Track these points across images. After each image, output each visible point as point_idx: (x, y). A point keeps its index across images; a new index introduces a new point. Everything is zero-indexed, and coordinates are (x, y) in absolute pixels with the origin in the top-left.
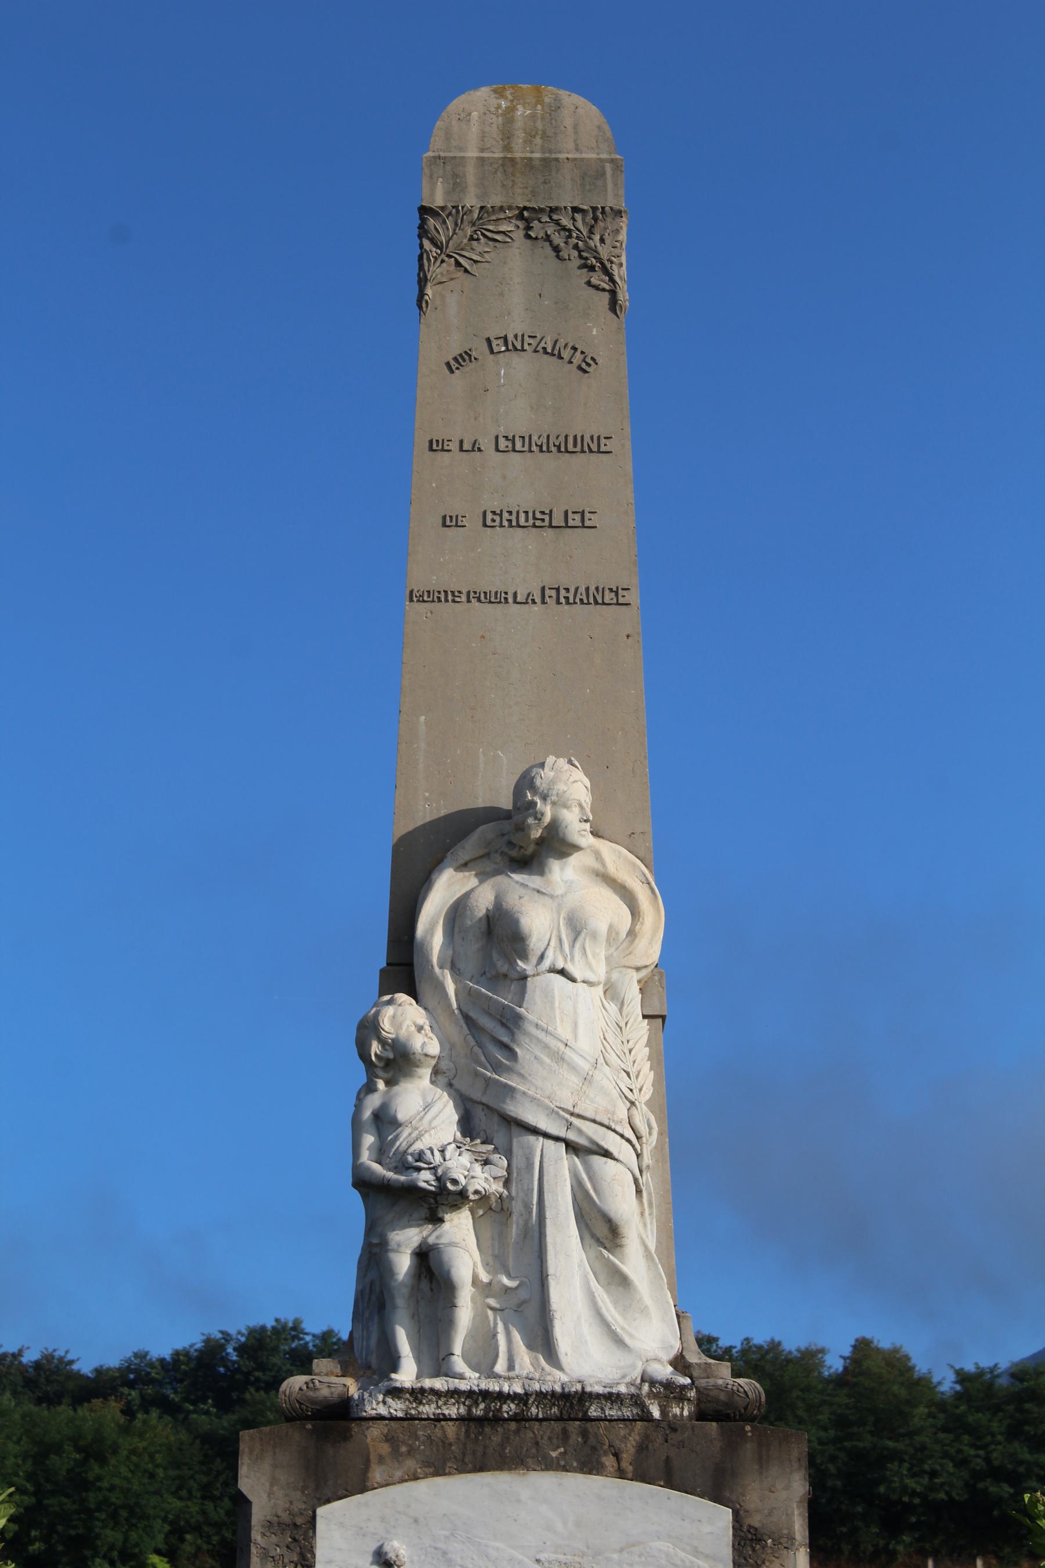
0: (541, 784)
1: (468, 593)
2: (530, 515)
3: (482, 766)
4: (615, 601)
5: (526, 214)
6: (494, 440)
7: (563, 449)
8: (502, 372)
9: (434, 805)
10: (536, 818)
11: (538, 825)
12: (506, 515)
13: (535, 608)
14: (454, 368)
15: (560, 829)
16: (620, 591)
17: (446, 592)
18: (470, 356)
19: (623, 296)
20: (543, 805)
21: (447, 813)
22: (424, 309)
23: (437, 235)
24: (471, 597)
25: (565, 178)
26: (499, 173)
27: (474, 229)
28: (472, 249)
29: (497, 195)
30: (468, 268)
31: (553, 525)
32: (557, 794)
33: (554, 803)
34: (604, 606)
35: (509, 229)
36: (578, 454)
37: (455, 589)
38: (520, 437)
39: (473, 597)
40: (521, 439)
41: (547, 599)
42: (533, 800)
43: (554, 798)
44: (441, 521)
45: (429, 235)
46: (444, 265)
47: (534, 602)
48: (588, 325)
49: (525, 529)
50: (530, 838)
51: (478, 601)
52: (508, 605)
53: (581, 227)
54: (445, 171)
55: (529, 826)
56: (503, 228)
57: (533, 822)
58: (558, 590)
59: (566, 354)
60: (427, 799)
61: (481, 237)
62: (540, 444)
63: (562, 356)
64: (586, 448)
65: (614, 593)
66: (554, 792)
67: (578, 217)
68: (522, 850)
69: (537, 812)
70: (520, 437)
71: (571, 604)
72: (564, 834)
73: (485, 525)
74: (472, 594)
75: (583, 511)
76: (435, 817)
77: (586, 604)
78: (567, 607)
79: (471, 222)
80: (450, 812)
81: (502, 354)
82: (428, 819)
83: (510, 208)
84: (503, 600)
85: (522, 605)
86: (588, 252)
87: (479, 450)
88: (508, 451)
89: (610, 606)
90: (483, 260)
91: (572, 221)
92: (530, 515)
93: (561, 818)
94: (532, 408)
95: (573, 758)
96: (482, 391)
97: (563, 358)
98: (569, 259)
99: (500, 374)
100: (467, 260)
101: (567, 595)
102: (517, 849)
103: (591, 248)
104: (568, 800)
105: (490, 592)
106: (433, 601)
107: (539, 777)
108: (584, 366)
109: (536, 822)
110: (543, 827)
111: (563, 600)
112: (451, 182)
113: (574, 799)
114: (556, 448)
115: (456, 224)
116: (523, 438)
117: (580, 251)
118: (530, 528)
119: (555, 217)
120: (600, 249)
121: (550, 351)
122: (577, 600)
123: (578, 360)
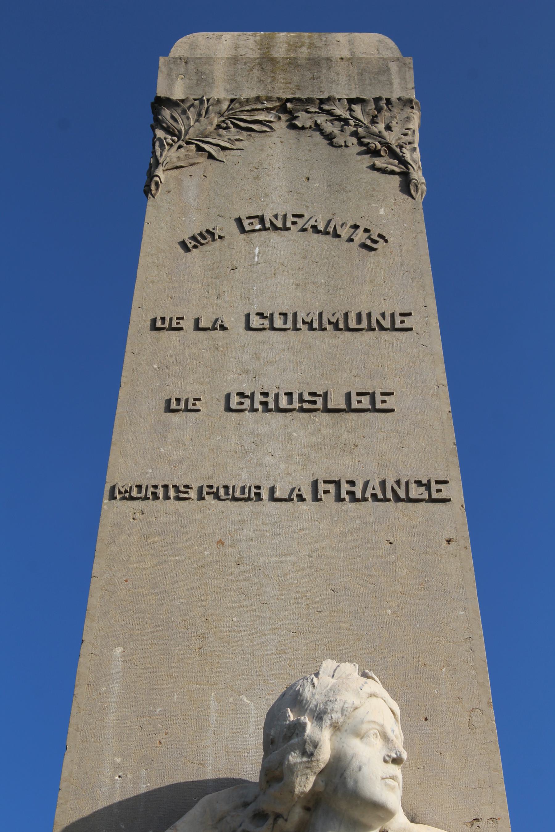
0: (313, 695)
1: (200, 489)
2: (296, 397)
3: (213, 717)
4: (426, 496)
5: (289, 105)
6: (244, 318)
7: (341, 325)
8: (257, 251)
9: (130, 776)
10: (304, 753)
11: (309, 766)
12: (259, 398)
13: (303, 506)
14: (190, 246)
15: (348, 772)
16: (433, 484)
17: (166, 487)
18: (212, 234)
19: (418, 175)
20: (317, 729)
21: (151, 789)
22: (153, 192)
23: (175, 124)
24: (204, 492)
25: (338, 74)
26: (255, 71)
27: (222, 119)
28: (220, 136)
29: (252, 89)
30: (214, 153)
31: (329, 407)
32: (342, 710)
33: (336, 727)
34: (410, 504)
35: (267, 119)
36: (364, 332)
37: (180, 484)
38: (280, 314)
39: (208, 493)
40: (282, 317)
41: (321, 493)
42: (298, 720)
43: (336, 716)
44: (163, 406)
45: (164, 125)
46: (182, 150)
47: (301, 498)
48: (374, 205)
49: (287, 415)
50: (292, 792)
51: (214, 498)
52: (261, 502)
53: (360, 116)
54: (187, 70)
55: (291, 769)
56: (261, 117)
57: (299, 760)
58: (338, 484)
59: (345, 233)
60: (117, 767)
61: (231, 126)
62: (309, 321)
63: (338, 233)
64: (374, 324)
65: (424, 488)
66: (337, 706)
67: (357, 108)
68: (280, 821)
69: (305, 742)
70: (280, 314)
71: (358, 500)
72: (356, 782)
73: (228, 409)
74: (206, 490)
75: (374, 393)
76: (130, 794)
77: (381, 500)
78: (353, 505)
79: (219, 113)
80: (155, 787)
81: (256, 234)
82: (118, 798)
83: (269, 99)
84: (252, 495)
85: (283, 503)
86: (369, 137)
87: (223, 328)
88: (264, 329)
89: (418, 504)
90: (233, 147)
91: (348, 113)
92: (296, 397)
93: (350, 752)
94: (298, 286)
95: (367, 671)
96: (228, 270)
97: (339, 236)
98: (346, 146)
99: (254, 252)
100: (213, 147)
101: (352, 489)
102: (270, 821)
103: (374, 134)
104: (362, 722)
105: (234, 487)
106: (146, 498)
107: (309, 684)
108: (369, 242)
109: (305, 759)
110: (318, 770)
111: (344, 495)
112: (194, 78)
113: (374, 722)
114: (332, 326)
115: (199, 115)
116: (285, 315)
117: (359, 138)
118: (295, 412)
119: (326, 107)
120: (386, 134)
121: (322, 229)
122: (368, 495)
123: (360, 239)
